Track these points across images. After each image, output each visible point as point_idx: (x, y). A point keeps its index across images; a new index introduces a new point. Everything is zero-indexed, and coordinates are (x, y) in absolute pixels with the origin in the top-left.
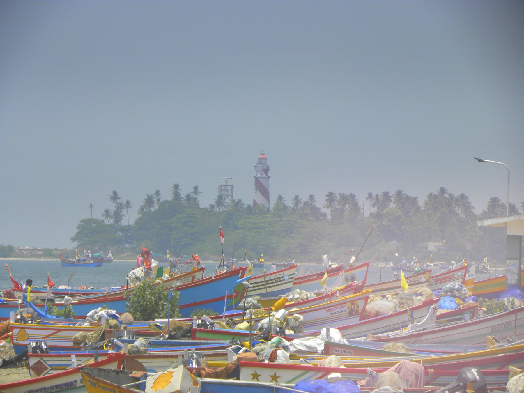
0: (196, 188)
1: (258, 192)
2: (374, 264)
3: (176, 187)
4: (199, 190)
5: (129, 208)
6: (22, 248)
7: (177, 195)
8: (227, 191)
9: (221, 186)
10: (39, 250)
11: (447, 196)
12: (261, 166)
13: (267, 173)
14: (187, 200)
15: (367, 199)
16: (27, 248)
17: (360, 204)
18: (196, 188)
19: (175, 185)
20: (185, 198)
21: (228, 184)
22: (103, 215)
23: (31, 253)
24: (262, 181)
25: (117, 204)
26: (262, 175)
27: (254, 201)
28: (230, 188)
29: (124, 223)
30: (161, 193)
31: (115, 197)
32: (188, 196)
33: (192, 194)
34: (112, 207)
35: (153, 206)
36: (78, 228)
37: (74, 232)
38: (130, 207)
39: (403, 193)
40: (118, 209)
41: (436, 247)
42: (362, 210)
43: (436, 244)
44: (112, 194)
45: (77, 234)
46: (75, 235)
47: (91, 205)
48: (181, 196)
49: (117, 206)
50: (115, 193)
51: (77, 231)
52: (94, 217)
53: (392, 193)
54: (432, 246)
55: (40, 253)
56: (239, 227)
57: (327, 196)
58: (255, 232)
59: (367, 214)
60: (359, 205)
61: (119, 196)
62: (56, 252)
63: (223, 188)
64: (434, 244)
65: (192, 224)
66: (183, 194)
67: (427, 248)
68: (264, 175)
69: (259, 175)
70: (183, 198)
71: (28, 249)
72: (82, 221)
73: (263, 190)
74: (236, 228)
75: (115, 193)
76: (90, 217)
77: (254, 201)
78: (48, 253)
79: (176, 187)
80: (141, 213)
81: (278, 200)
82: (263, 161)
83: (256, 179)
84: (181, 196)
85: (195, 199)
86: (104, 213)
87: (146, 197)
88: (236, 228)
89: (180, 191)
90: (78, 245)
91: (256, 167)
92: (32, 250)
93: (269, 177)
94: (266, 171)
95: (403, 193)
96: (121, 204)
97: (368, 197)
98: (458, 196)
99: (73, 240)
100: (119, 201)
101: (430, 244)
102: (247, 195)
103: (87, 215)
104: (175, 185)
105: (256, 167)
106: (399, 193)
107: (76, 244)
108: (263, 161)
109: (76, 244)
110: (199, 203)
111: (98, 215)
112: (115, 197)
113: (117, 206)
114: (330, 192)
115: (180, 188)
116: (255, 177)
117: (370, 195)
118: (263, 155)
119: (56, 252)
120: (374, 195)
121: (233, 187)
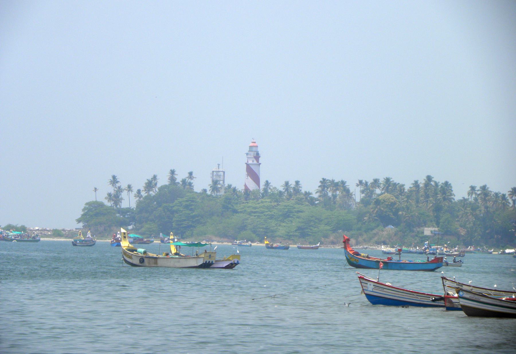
0: (191, 174)
1: (249, 177)
2: (374, 247)
3: (173, 172)
4: (194, 175)
5: (130, 192)
6: (32, 229)
7: (172, 179)
8: (219, 176)
9: (213, 172)
10: (48, 230)
11: (433, 183)
12: (252, 153)
13: (257, 160)
14: (183, 184)
15: (358, 185)
16: (37, 228)
17: (351, 190)
18: (191, 174)
19: (171, 170)
20: (181, 183)
21: (221, 169)
22: (106, 198)
23: (41, 233)
24: (252, 167)
25: (116, 188)
26: (253, 161)
27: (245, 186)
28: (222, 173)
29: (124, 205)
30: (157, 178)
31: (114, 181)
32: (184, 181)
33: (187, 179)
34: (111, 190)
35: (152, 190)
36: (83, 210)
37: (79, 214)
38: (132, 191)
39: (391, 180)
40: (117, 192)
41: (432, 232)
42: (354, 196)
43: (433, 229)
44: (112, 179)
45: (82, 215)
46: (80, 216)
47: (96, 189)
48: (177, 181)
49: (115, 189)
50: (114, 177)
51: (82, 213)
52: (99, 200)
53: (382, 180)
54: (427, 231)
55: (50, 233)
56: (239, 211)
57: (321, 182)
58: (255, 216)
59: (358, 200)
60: (351, 191)
61: (118, 180)
62: (64, 233)
63: (215, 173)
64: (430, 229)
65: (193, 207)
66: (179, 180)
67: (423, 233)
68: (255, 162)
69: (250, 162)
70: (178, 183)
71: (38, 230)
72: (87, 204)
73: (256, 178)
74: (235, 211)
75: (114, 177)
76: (95, 200)
77: (245, 186)
78: (57, 233)
79: (173, 172)
80: (138, 196)
81: (265, 185)
82: (254, 149)
83: (248, 165)
84: (177, 181)
85: (190, 184)
86: (107, 196)
87: (147, 181)
88: (235, 211)
89: (176, 176)
90: (83, 226)
91: (247, 154)
92: (41, 230)
93: (260, 164)
94: (257, 157)
95: (391, 180)
96: (119, 187)
97: (358, 183)
98: (442, 184)
99: (79, 221)
100: (118, 185)
101: (426, 229)
102: (238, 180)
103: (91, 198)
104: (171, 170)
105: (247, 154)
106: (388, 180)
107: (81, 225)
108: (254, 149)
109: (81, 225)
110: (194, 188)
111: (102, 197)
112: (114, 181)
113: (115, 189)
114: (323, 179)
115: (176, 173)
116: (246, 164)
117: (361, 182)
118: (255, 142)
119: (64, 233)
120: (364, 182)
121: (224, 172)
